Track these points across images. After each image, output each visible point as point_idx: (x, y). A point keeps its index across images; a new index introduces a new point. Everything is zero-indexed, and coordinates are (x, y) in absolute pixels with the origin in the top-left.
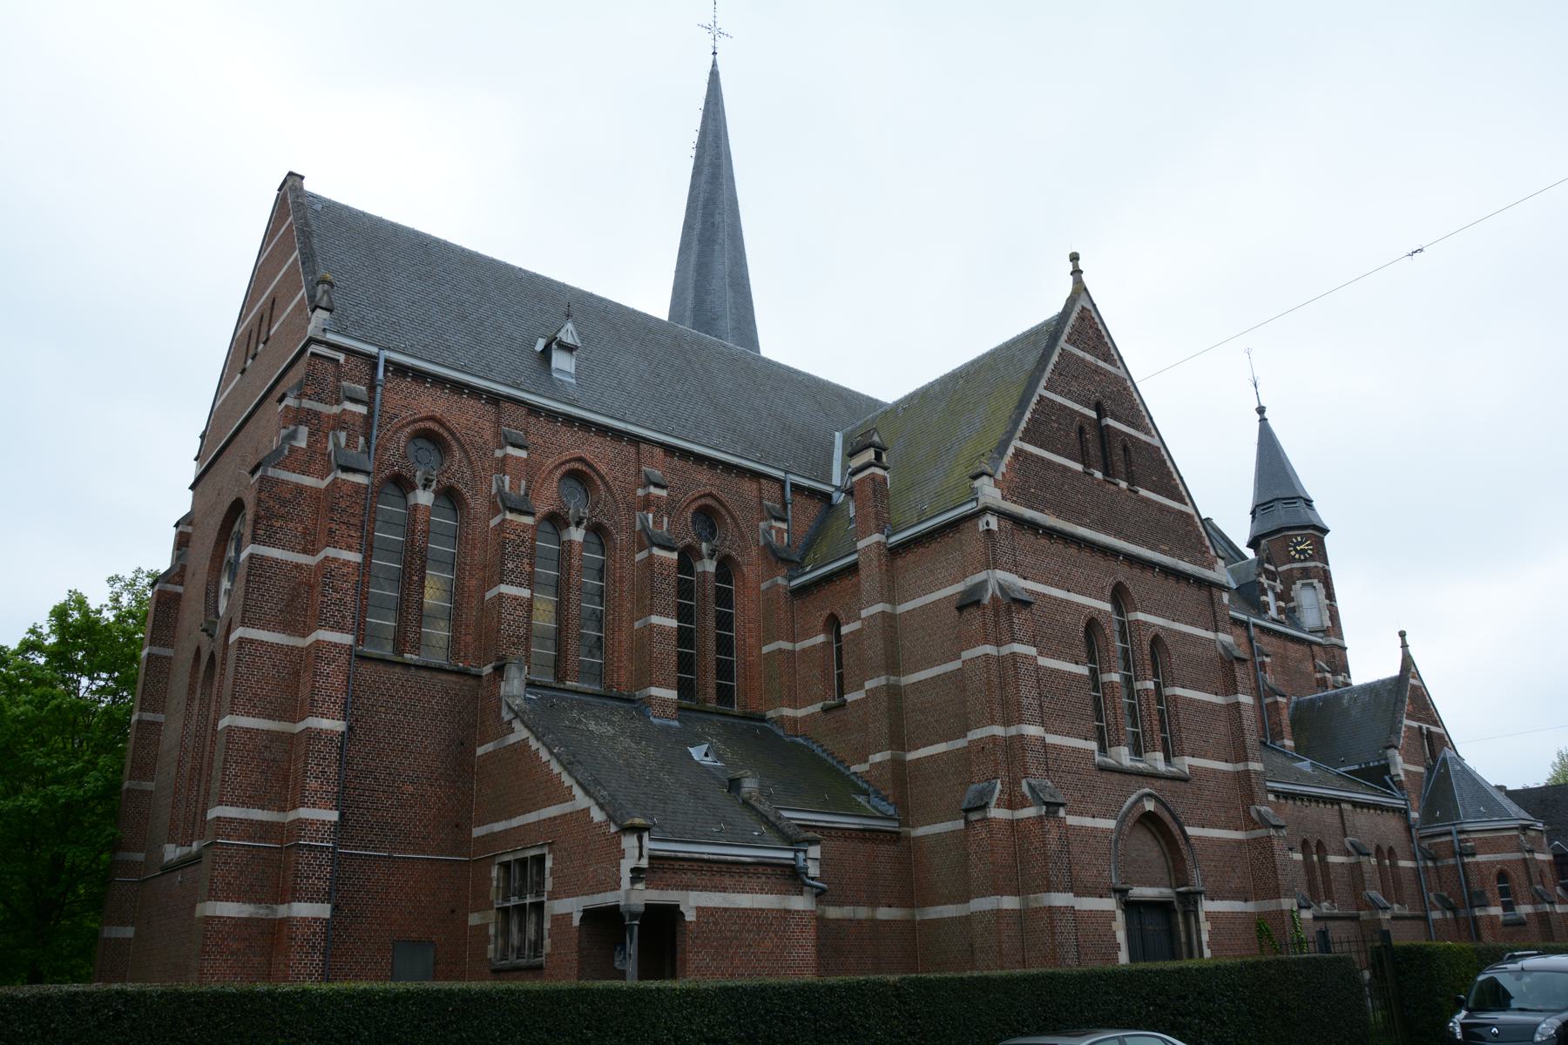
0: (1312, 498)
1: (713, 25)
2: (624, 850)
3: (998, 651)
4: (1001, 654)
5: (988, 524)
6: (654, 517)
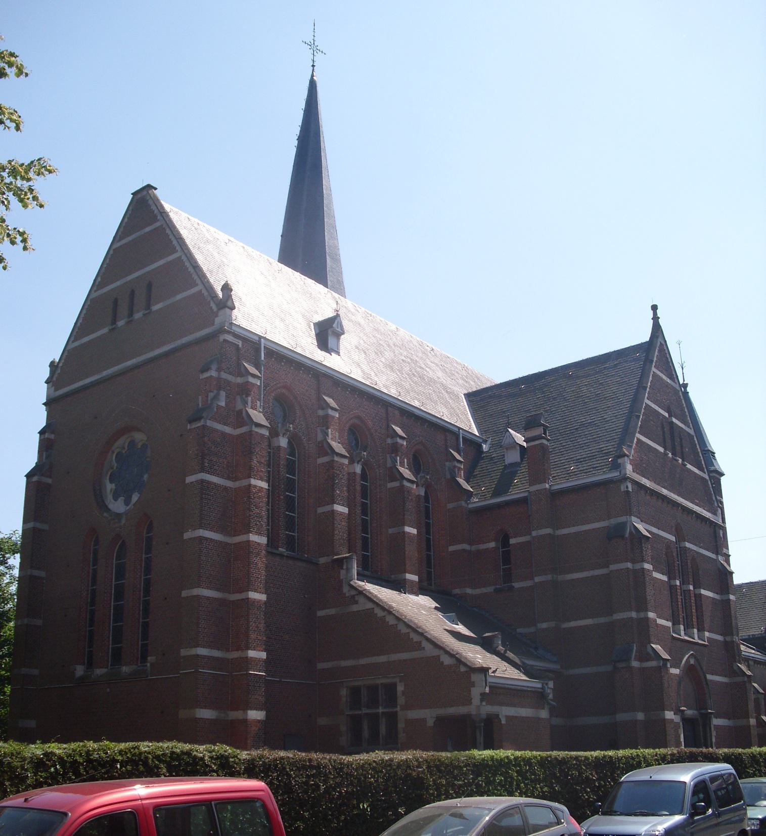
0: (715, 451)
1: (312, 43)
2: (474, 682)
3: (633, 567)
4: (635, 568)
5: (627, 487)
6: (400, 458)
